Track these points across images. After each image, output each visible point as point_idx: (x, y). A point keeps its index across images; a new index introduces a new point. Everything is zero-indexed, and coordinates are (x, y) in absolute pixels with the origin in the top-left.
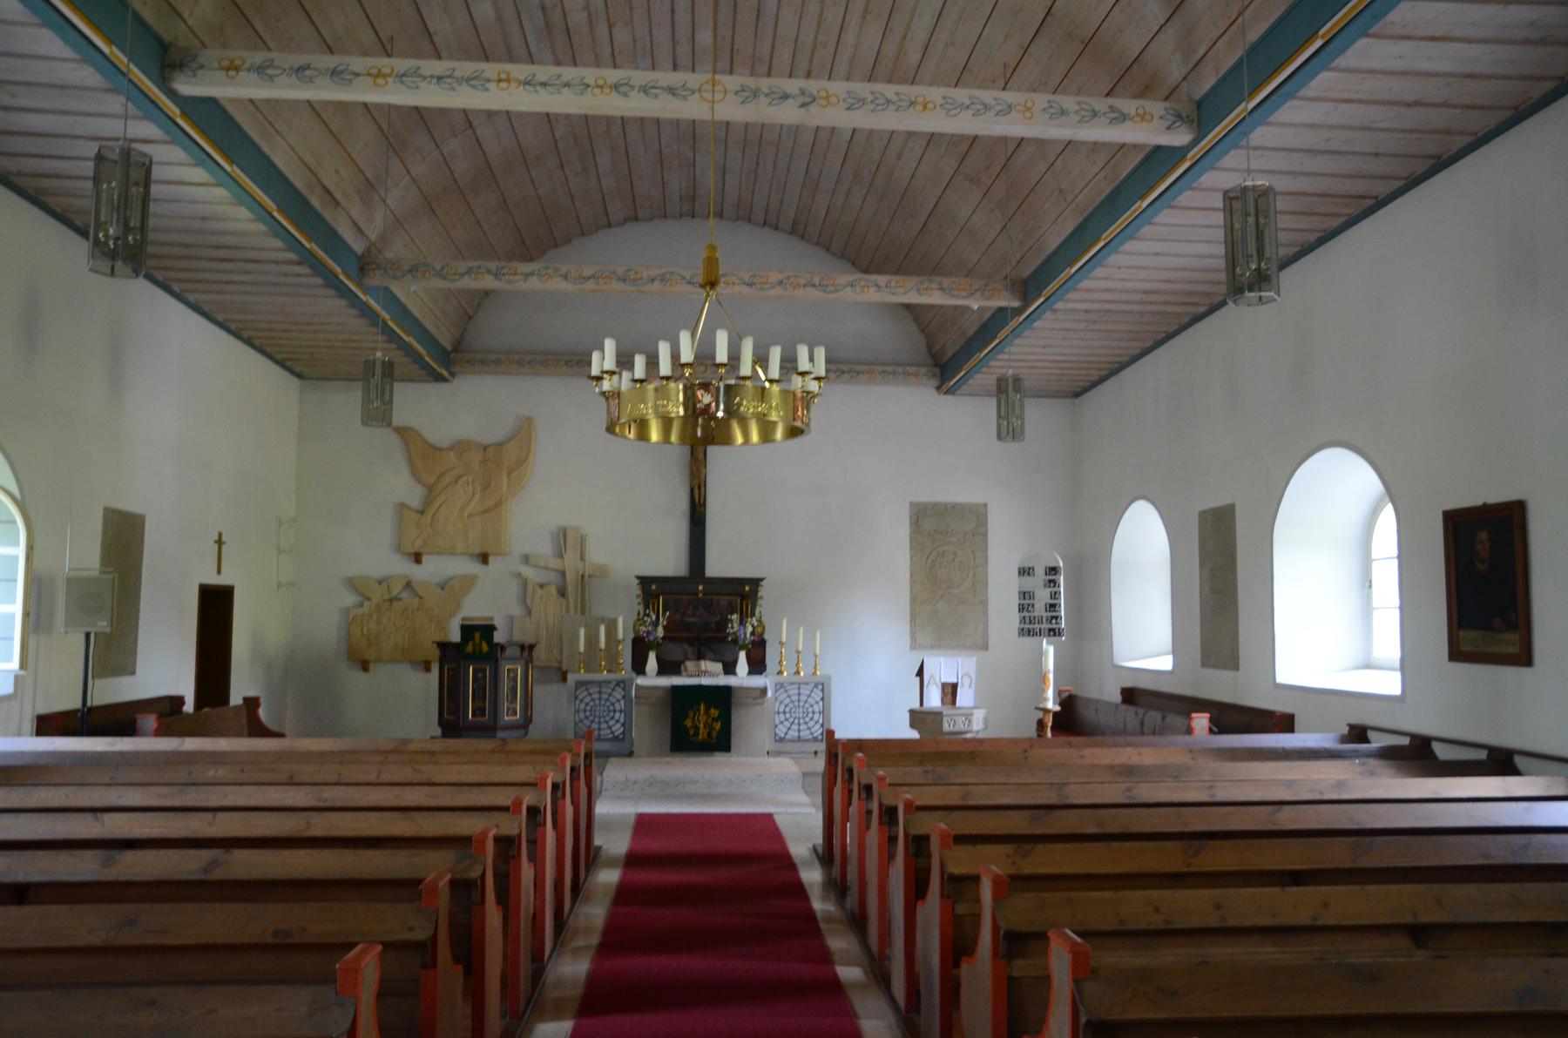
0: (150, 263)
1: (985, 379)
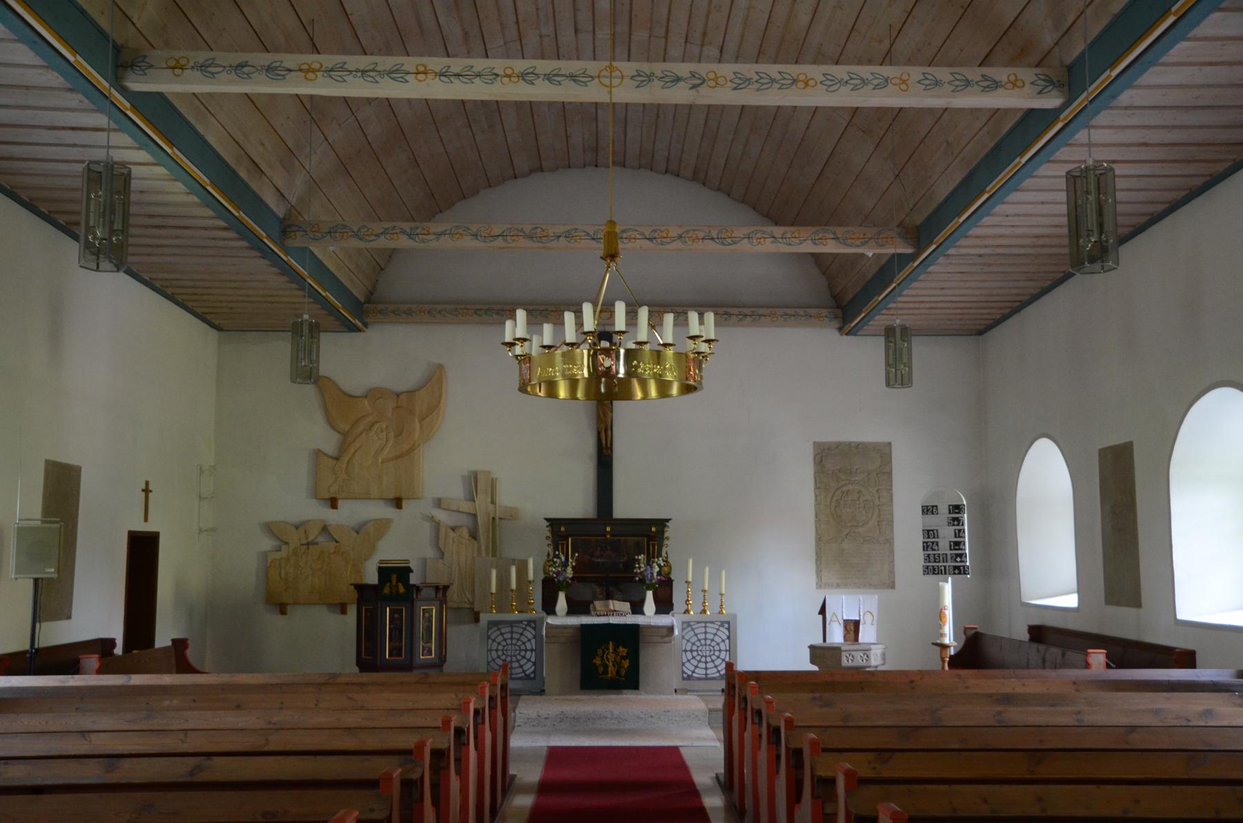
0: (130, 259)
1: (881, 320)
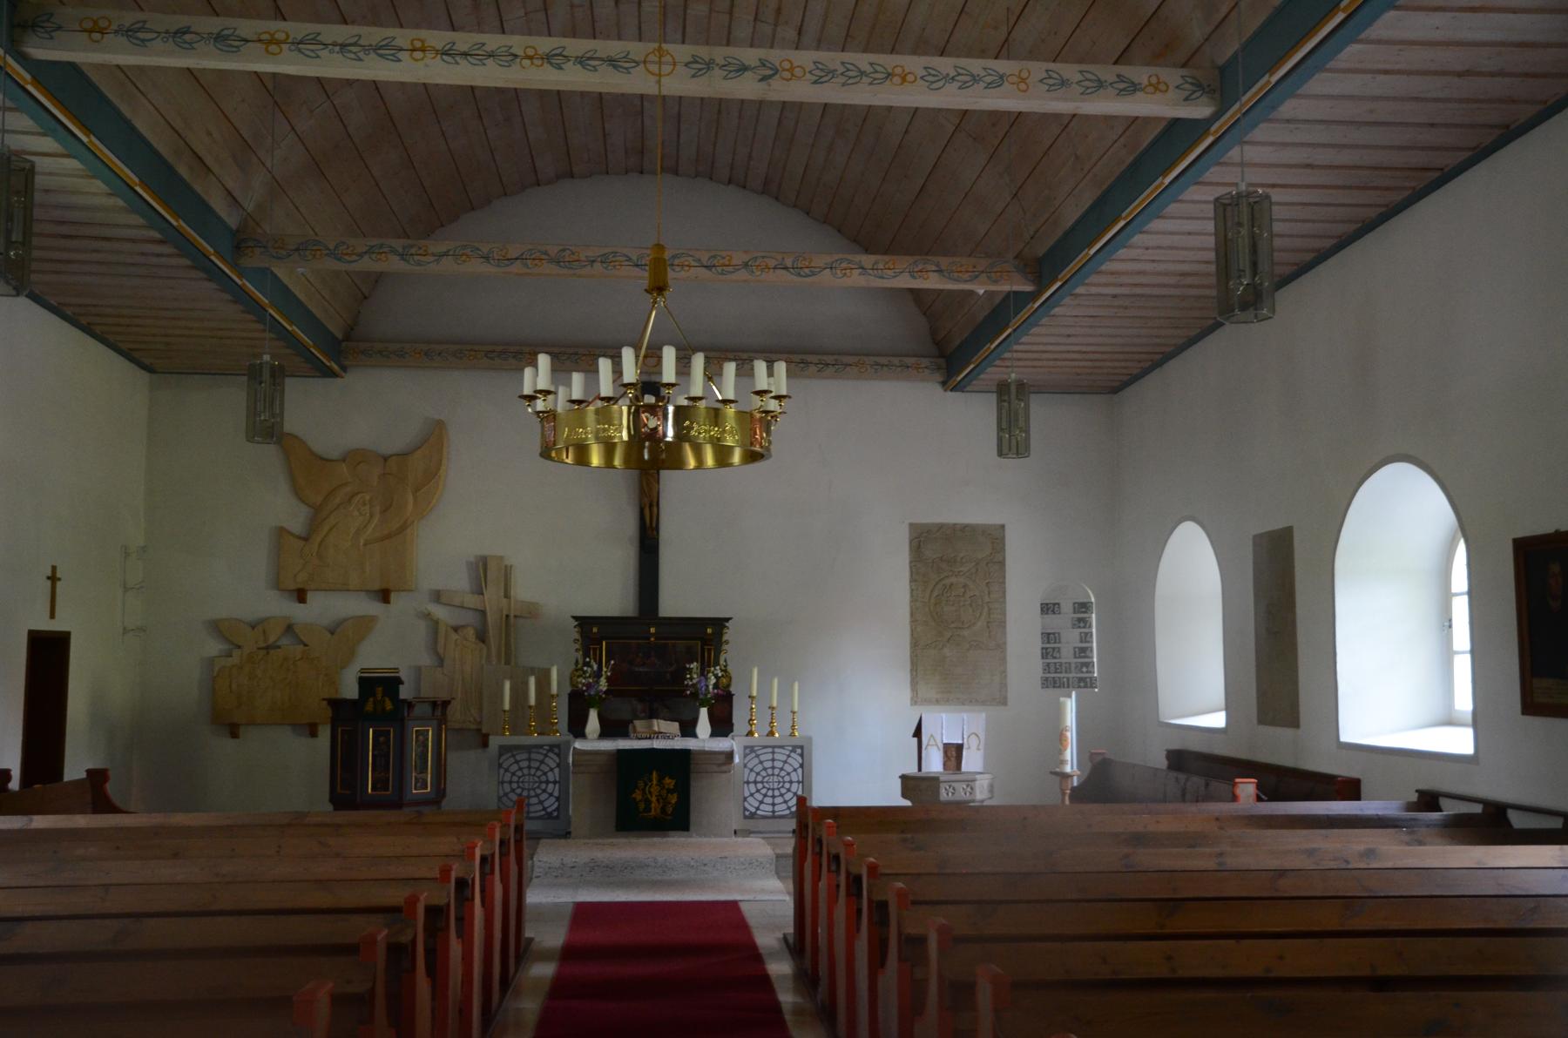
0: (34, 277)
1: (993, 374)
